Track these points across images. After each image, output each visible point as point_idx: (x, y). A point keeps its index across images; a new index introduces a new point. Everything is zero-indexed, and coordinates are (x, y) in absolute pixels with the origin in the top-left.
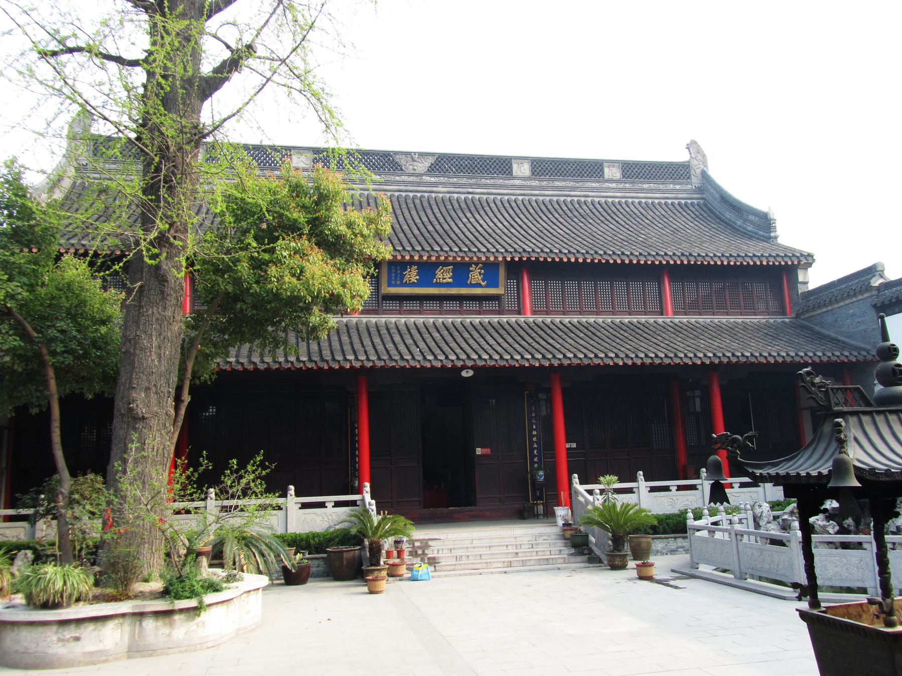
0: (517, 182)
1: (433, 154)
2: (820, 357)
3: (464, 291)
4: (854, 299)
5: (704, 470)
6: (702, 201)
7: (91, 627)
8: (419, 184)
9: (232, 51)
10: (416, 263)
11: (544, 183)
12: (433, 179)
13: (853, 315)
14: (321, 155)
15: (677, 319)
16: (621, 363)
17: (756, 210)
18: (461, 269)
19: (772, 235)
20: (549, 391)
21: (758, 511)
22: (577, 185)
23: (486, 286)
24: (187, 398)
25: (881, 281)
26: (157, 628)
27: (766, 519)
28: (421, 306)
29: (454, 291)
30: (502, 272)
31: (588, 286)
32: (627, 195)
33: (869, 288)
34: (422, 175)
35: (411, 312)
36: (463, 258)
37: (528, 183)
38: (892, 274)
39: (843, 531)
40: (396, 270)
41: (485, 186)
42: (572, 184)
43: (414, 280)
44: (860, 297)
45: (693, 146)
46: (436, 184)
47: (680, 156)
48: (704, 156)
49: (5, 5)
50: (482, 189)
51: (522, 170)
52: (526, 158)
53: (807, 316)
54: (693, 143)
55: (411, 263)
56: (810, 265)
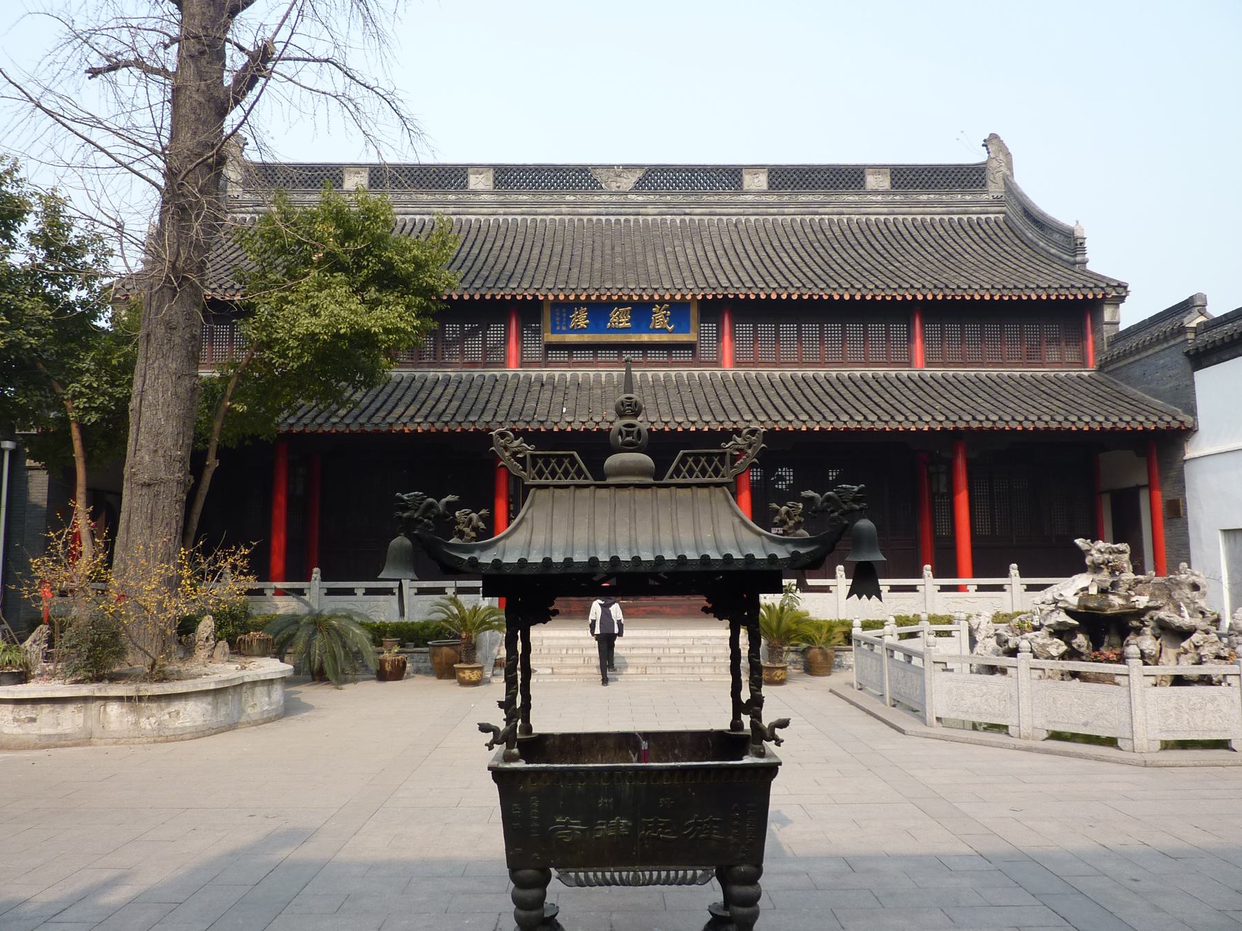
0: (750, 198)
1: (641, 167)
2: (1101, 423)
3: (645, 338)
4: (1166, 345)
5: (1015, 566)
6: (1001, 216)
7: (46, 709)
8: (623, 204)
9: (248, 53)
10: (583, 304)
11: (786, 198)
12: (640, 198)
13: (1164, 366)
14: (379, 175)
15: (928, 373)
16: (926, 428)
17: (1062, 225)
18: (641, 310)
19: (1079, 258)
20: (951, 465)
21: (974, 622)
22: (828, 199)
23: (672, 332)
24: (212, 463)
25: (1202, 319)
26: (121, 715)
27: (984, 633)
28: (595, 355)
29: (634, 338)
30: (694, 312)
31: (854, 329)
32: (896, 210)
33: (1182, 330)
34: (626, 193)
35: (581, 364)
36: (641, 296)
37: (764, 198)
38: (1216, 309)
39: (1072, 654)
40: (561, 313)
41: (708, 204)
42: (821, 198)
43: (582, 324)
44: (1172, 342)
45: (992, 141)
46: (644, 204)
47: (974, 155)
48: (1008, 154)
49: (299, 3)
50: (556, 211)
51: (759, 182)
52: (762, 167)
53: (1111, 368)
54: (994, 137)
55: (577, 304)
56: (1122, 299)
